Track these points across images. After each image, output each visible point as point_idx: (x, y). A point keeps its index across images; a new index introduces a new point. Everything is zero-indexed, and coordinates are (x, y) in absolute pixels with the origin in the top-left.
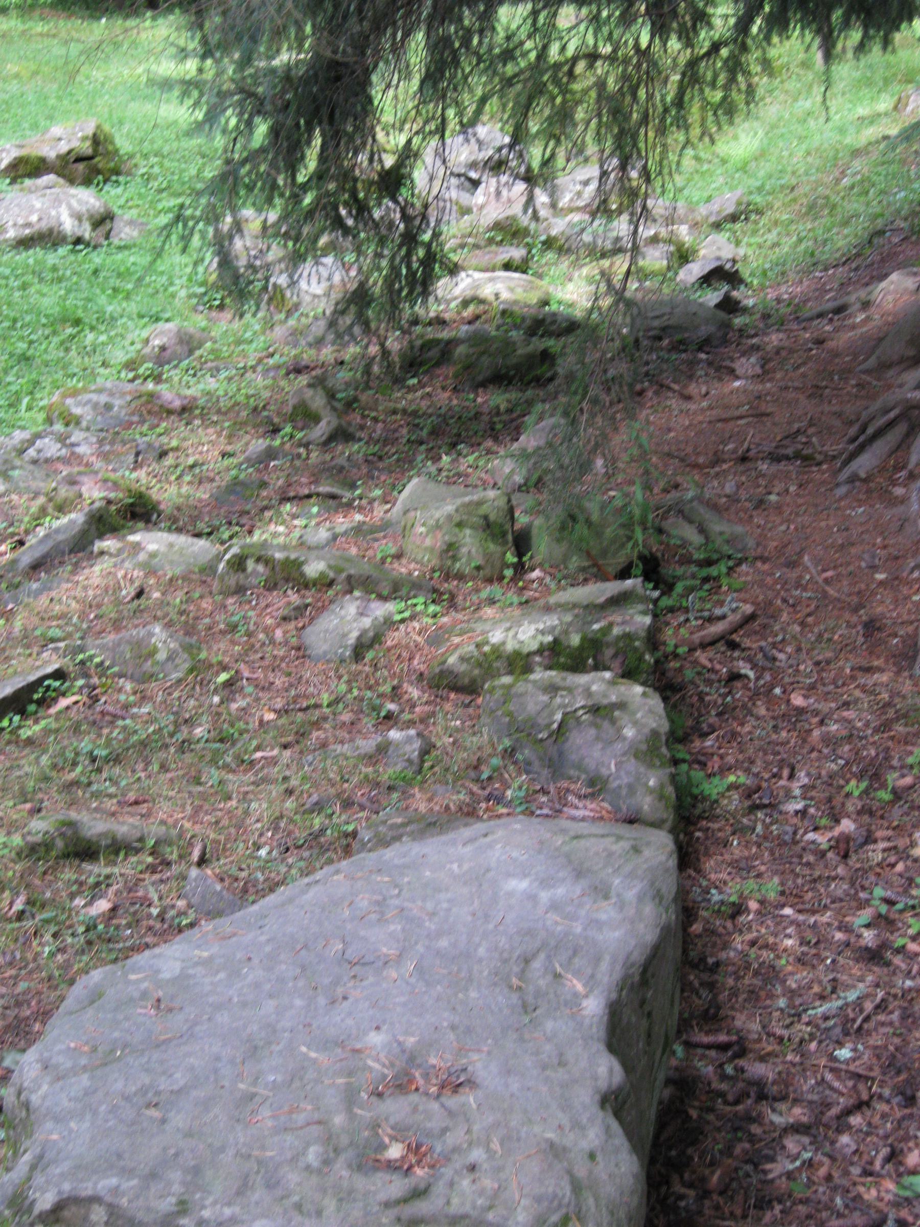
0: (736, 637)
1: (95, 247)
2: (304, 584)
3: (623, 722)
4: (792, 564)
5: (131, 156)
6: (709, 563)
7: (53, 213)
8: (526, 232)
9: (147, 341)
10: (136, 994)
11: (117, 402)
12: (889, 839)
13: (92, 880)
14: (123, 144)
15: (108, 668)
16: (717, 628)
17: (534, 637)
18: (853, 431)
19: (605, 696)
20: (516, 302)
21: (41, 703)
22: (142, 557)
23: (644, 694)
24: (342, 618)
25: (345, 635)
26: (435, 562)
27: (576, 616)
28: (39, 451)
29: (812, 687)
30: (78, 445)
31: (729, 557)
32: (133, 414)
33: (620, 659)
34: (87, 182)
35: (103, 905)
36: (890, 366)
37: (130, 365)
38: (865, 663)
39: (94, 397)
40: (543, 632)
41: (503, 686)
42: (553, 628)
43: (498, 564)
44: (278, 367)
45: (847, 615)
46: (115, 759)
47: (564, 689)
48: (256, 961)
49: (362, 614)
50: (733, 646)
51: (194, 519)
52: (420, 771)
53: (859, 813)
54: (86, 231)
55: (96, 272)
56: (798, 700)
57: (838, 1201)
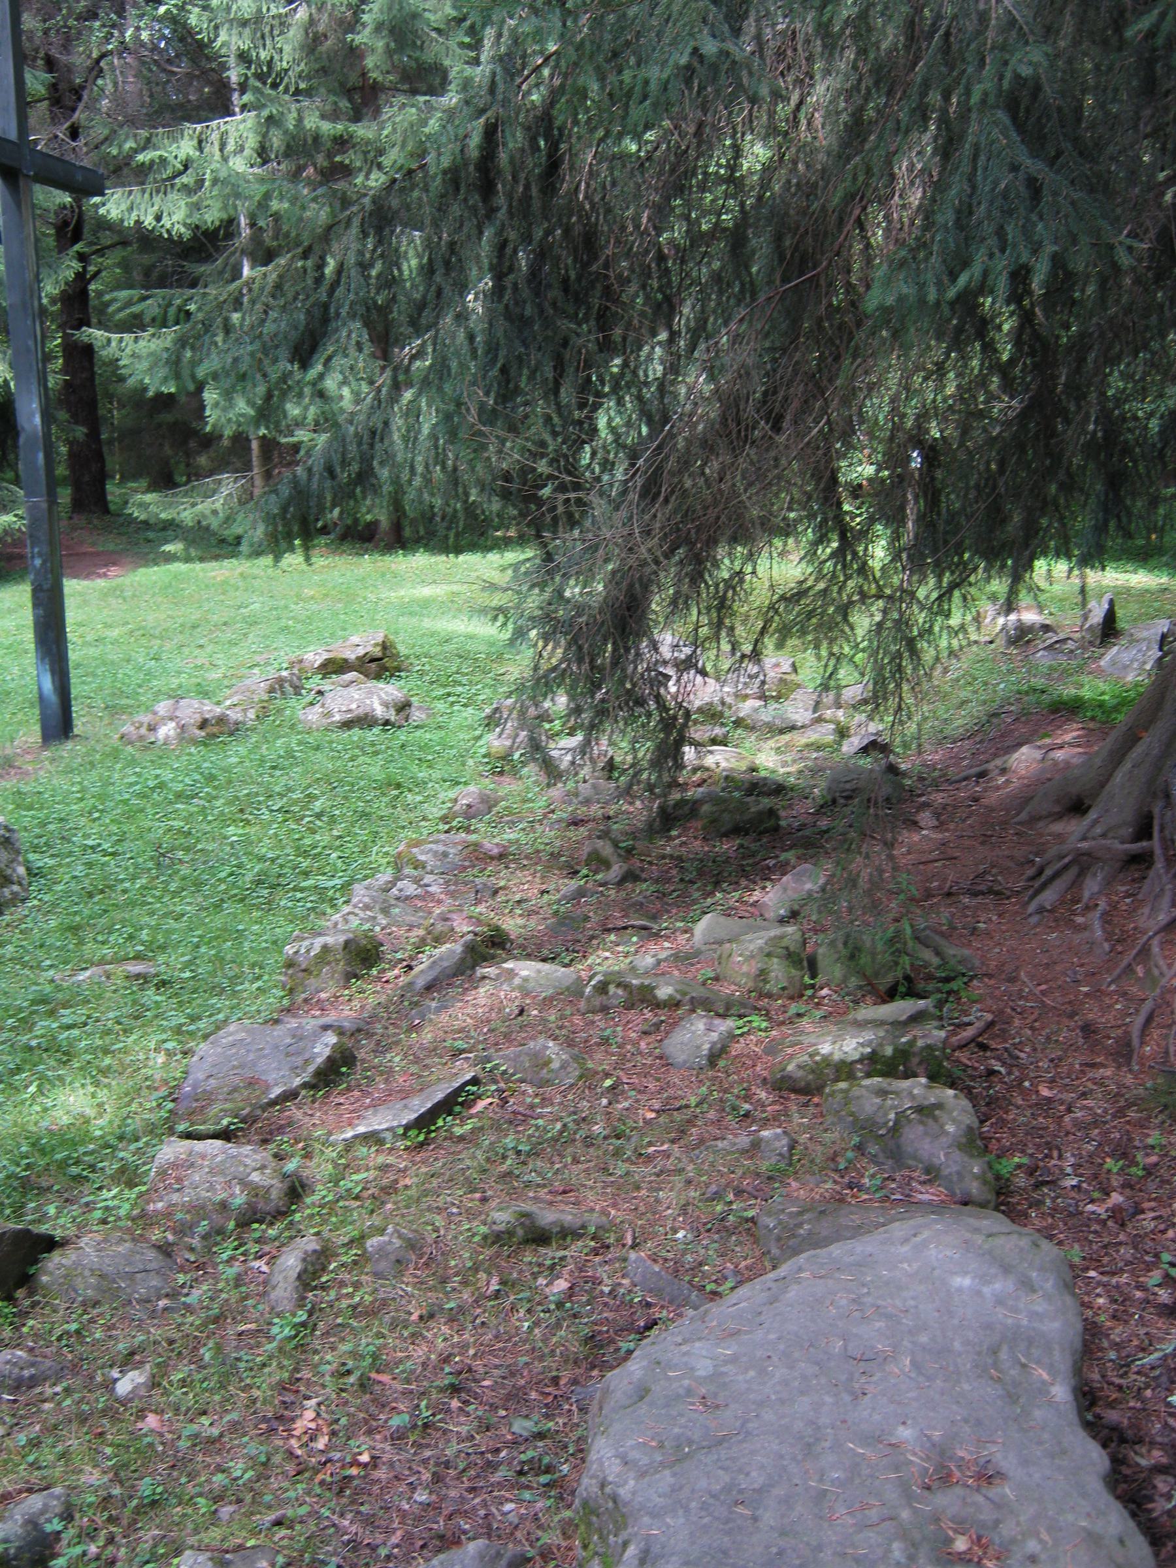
2: (657, 1005)
4: (1012, 980)
5: (408, 657)
6: (947, 980)
8: (721, 715)
9: (456, 801)
10: (681, 1391)
12: (1153, 1209)
13: (548, 1262)
14: (402, 650)
15: (513, 1075)
16: (969, 1032)
18: (1030, 872)
20: (732, 769)
22: (517, 981)
23: (956, 1096)
24: (693, 1032)
25: (698, 1047)
26: (750, 984)
28: (401, 890)
29: (1052, 1081)
31: (964, 975)
34: (378, 677)
35: (561, 1285)
36: (1040, 818)
37: (444, 819)
38: (1088, 1060)
40: (862, 1045)
41: (842, 1091)
42: (871, 1041)
43: (798, 985)
44: (559, 821)
45: (1066, 1021)
46: (534, 1153)
47: (892, 1093)
48: (775, 1359)
50: (984, 1047)
51: (539, 946)
52: (790, 1165)
53: (1123, 1186)
54: (392, 716)
55: (403, 746)
56: (1045, 1092)
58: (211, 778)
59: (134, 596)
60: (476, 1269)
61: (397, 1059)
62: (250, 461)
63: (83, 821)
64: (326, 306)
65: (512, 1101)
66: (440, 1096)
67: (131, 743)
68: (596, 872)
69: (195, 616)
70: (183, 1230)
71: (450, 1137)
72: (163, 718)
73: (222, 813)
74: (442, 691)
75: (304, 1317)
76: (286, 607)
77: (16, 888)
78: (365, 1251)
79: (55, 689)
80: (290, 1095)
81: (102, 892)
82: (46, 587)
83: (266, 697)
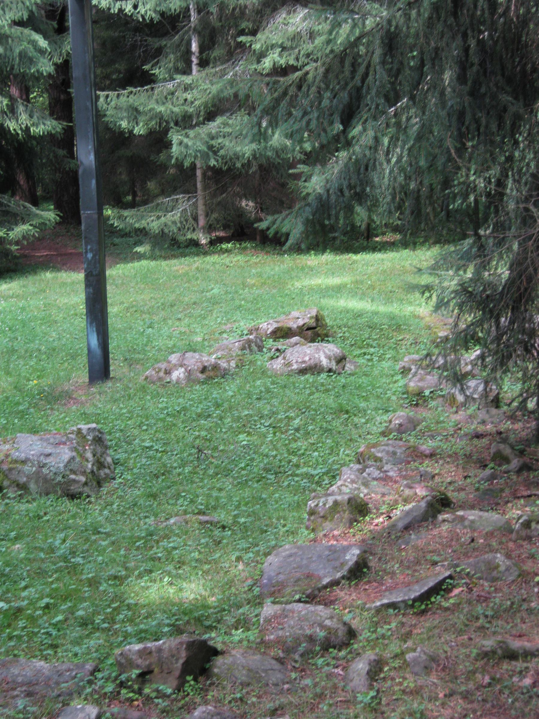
1: (339, 374)
5: (332, 327)
7: (317, 356)
9: (390, 421)
11: (399, 451)
14: (329, 322)
28: (369, 474)
32: (408, 456)
34: (313, 341)
44: (466, 435)
58: (217, 406)
59: (123, 284)
60: (474, 672)
61: (397, 565)
62: (195, 185)
63: (136, 432)
64: (359, 90)
65: (475, 589)
66: (431, 584)
67: (153, 383)
68: (500, 465)
69: (172, 298)
70: (288, 651)
71: (440, 607)
72: (175, 365)
73: (231, 427)
74: (358, 352)
75: (375, 694)
76: (236, 292)
77: (107, 471)
78: (405, 660)
79: (99, 344)
80: (335, 583)
81: (163, 474)
82: (94, 273)
83: (240, 353)
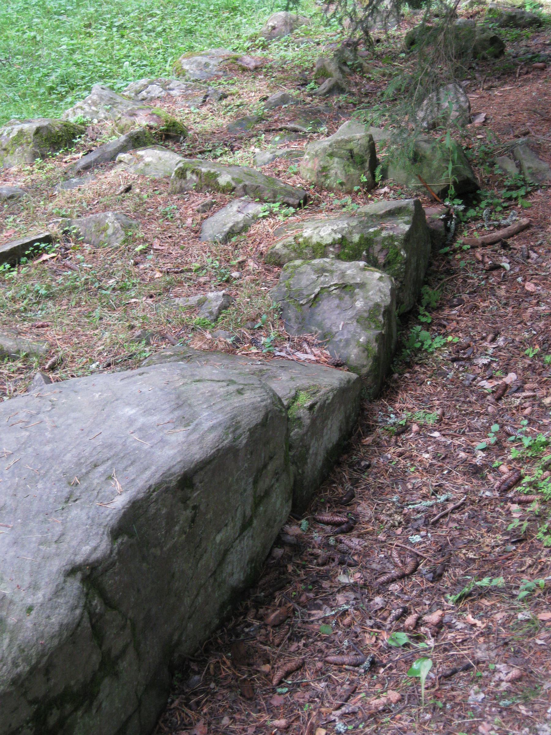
0: (509, 241)
2: (217, 188)
3: (357, 297)
12: (533, 390)
17: (330, 234)
19: (353, 278)
21: (29, 257)
22: (141, 165)
23: (381, 279)
25: (224, 225)
26: (314, 179)
27: (360, 222)
28: (149, 92)
30: (173, 89)
33: (384, 253)
39: (199, 59)
40: (335, 232)
42: (343, 229)
46: (50, 296)
49: (239, 212)
52: (216, 320)
57: (346, 643)
